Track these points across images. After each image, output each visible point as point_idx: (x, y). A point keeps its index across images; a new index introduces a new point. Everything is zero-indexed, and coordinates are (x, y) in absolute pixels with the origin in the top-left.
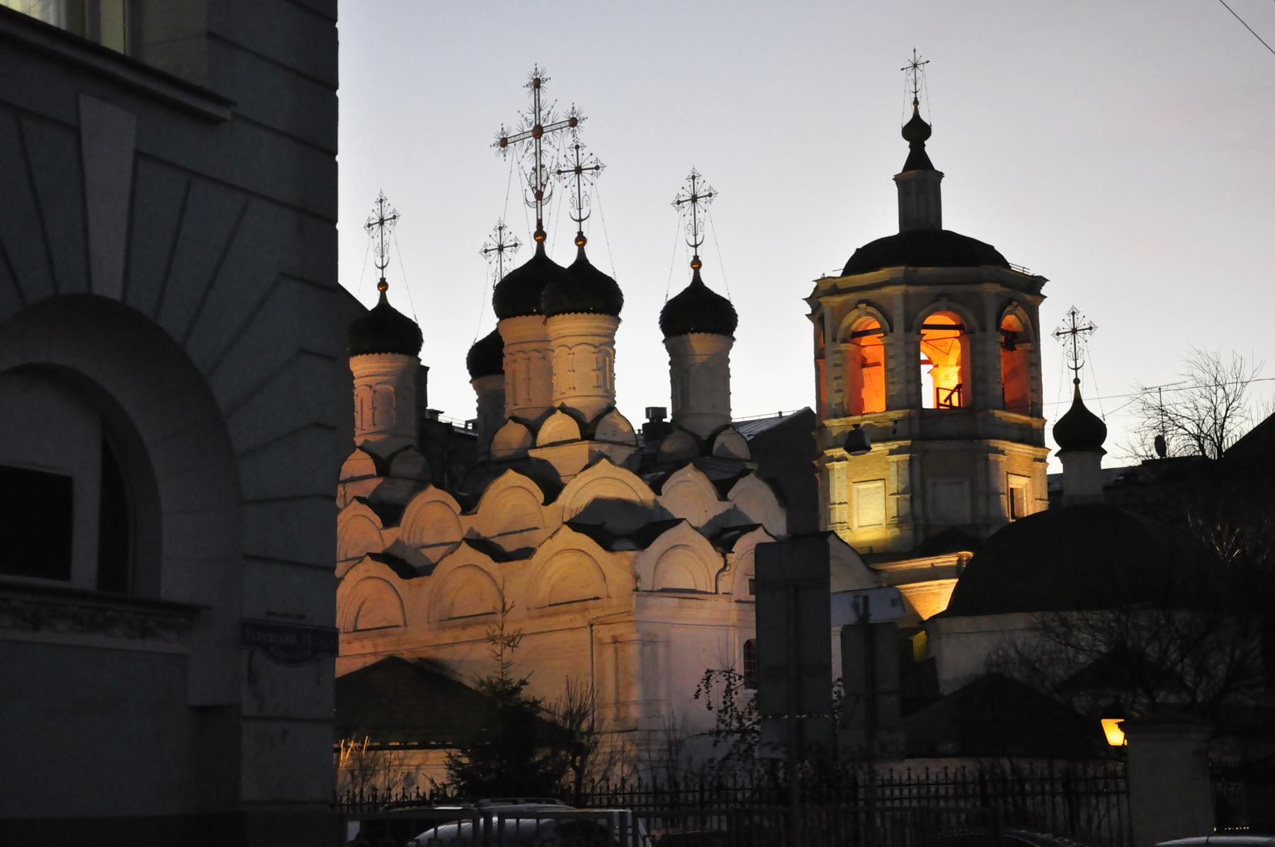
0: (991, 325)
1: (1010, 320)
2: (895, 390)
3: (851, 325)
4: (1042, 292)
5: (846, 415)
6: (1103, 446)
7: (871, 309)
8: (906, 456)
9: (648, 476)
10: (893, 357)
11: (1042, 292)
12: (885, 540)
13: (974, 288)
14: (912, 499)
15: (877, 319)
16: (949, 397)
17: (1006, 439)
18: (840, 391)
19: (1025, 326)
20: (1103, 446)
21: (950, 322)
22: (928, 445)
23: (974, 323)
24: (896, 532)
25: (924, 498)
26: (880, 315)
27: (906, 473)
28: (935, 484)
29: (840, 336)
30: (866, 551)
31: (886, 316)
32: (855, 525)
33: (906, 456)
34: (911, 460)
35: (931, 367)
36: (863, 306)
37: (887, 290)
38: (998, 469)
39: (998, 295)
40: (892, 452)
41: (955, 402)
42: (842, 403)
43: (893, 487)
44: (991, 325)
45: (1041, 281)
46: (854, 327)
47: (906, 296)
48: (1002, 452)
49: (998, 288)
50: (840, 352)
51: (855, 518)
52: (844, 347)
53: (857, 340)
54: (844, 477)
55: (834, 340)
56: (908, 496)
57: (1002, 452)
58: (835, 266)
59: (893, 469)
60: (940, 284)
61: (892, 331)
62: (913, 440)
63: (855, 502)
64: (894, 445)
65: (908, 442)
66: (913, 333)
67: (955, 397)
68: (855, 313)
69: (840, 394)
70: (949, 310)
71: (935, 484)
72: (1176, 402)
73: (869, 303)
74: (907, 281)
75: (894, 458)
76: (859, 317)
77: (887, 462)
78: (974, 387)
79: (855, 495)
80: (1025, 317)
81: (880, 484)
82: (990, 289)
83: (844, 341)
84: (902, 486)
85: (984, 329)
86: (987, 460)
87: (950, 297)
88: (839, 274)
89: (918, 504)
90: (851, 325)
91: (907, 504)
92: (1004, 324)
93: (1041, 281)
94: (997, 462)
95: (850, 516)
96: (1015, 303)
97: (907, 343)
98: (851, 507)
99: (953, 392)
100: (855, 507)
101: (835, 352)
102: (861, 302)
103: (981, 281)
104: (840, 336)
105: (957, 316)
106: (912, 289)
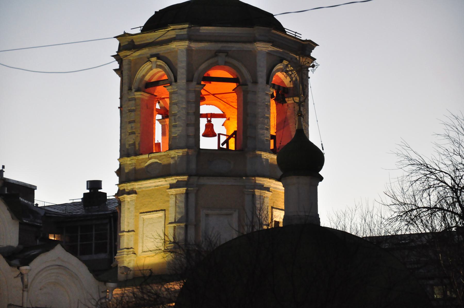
0: (262, 80)
1: (281, 77)
2: (177, 132)
3: (144, 76)
4: (312, 55)
5: (136, 154)
6: (320, 173)
7: (160, 62)
8: (183, 190)
9: (87, 257)
10: (176, 104)
11: (312, 55)
12: (163, 263)
13: (248, 46)
14: (186, 226)
15: (165, 70)
16: (227, 142)
17: (270, 177)
18: (133, 133)
19: (295, 83)
20: (320, 173)
21: (227, 75)
22: (204, 181)
23: (248, 76)
24: (169, 257)
25: (197, 226)
26: (167, 67)
27: (182, 205)
28: (207, 215)
29: (135, 85)
30: (148, 274)
31: (172, 68)
32: (139, 250)
33: (183, 190)
34: (187, 194)
35: (224, 120)
36: (154, 59)
37: (174, 45)
38: (262, 203)
39: (269, 54)
40: (172, 186)
41: (232, 146)
42: (134, 144)
43: (171, 217)
44: (262, 80)
45: (311, 45)
46: (147, 78)
47: (189, 51)
48: (268, 189)
49: (268, 47)
50: (135, 99)
51: (140, 244)
52: (138, 95)
53: (151, 89)
54: (132, 209)
55: (130, 89)
56: (183, 225)
57: (268, 189)
58: (134, 24)
59: (172, 201)
60: (216, 41)
61: (176, 81)
62: (190, 176)
63: (140, 230)
64: (173, 180)
65: (185, 178)
66: (194, 83)
67: (232, 142)
68: (147, 66)
69: (133, 136)
70: (226, 65)
71: (207, 215)
72: (432, 157)
73: (159, 57)
74: (190, 38)
75: (173, 191)
76: (151, 69)
77: (168, 195)
78: (245, 131)
79: (141, 225)
80: (295, 75)
81: (161, 214)
82: (263, 47)
83: (138, 90)
84: (179, 216)
85: (255, 82)
86: (253, 195)
87: (227, 53)
88: (138, 31)
89: (192, 231)
90: (144, 76)
91: (182, 232)
92: (274, 80)
93: (311, 45)
94: (262, 198)
95: (136, 243)
96: (285, 62)
97: (188, 91)
98: (137, 235)
99: (229, 137)
100: (140, 236)
101: (130, 100)
102: (152, 56)
103: (254, 40)
104: (135, 85)
105: (234, 71)
106: (195, 46)
